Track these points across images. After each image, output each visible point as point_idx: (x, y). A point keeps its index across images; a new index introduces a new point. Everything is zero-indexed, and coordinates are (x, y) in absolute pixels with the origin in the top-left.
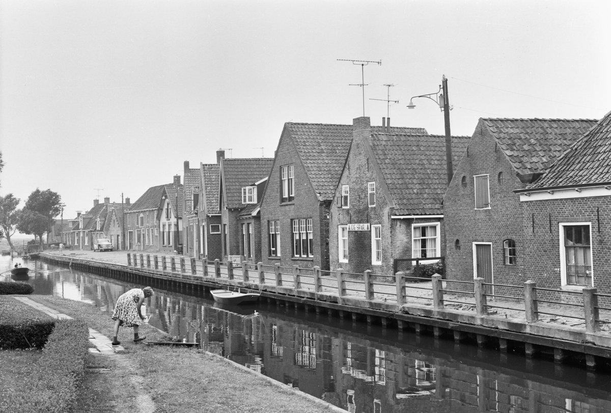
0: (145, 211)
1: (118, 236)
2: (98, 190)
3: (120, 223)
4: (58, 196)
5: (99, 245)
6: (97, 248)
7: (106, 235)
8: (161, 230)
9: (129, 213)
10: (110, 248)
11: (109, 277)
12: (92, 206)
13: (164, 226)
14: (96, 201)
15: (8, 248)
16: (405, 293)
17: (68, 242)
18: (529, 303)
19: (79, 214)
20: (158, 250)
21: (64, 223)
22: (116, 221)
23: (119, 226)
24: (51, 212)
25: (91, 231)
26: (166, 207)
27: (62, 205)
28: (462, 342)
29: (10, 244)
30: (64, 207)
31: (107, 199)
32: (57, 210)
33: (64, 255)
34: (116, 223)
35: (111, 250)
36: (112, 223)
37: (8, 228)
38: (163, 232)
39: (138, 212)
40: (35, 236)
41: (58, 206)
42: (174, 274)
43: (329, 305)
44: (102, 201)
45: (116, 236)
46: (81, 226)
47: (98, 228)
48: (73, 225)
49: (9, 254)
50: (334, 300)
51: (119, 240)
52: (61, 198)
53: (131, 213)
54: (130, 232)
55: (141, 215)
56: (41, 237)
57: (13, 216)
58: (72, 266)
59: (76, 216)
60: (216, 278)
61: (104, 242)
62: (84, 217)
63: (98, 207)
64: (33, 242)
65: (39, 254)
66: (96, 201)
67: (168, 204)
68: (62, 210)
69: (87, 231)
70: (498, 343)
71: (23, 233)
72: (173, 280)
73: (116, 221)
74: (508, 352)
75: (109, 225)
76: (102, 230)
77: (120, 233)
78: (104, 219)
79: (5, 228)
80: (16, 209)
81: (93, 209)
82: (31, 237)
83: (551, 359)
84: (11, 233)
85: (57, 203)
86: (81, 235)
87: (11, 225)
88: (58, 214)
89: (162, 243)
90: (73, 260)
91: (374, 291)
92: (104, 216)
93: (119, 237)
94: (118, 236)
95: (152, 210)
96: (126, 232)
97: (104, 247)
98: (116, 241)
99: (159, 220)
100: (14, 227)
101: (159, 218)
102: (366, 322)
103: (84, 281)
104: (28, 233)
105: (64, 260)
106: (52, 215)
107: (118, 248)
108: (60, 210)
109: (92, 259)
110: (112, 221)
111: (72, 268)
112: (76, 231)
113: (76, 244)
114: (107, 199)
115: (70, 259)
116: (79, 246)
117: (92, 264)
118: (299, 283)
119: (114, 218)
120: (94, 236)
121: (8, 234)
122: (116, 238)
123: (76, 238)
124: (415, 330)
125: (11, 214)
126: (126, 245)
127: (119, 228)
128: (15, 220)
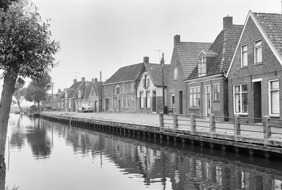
0: (121, 83)
1: (96, 102)
2: (76, 73)
3: (97, 93)
4: (50, 77)
5: (83, 108)
6: (81, 110)
7: (86, 101)
8: (138, 96)
9: (106, 86)
10: (91, 110)
11: (84, 128)
12: (72, 83)
13: (141, 93)
14: (75, 80)
15: (18, 110)
16: (163, 122)
17: (53, 107)
18: (53, 112)
19: (59, 91)
20: (134, 111)
21: (51, 96)
22: (94, 91)
23: (97, 95)
24: (45, 88)
25: (74, 99)
26: (144, 79)
27: (52, 83)
28: (226, 151)
29: (20, 107)
30: (53, 85)
31: (83, 79)
32: (49, 86)
33: (62, 114)
34: (94, 93)
35: (91, 112)
36: (91, 93)
37: (18, 98)
38: (140, 98)
39: (114, 84)
40: (35, 103)
41: (50, 84)
42: (176, 130)
43: (183, 136)
44: (79, 80)
45: (94, 102)
46: (66, 96)
47: (79, 97)
48: (56, 96)
49: (19, 113)
50: (188, 133)
51: (97, 104)
52: (52, 78)
53: (108, 85)
54: (106, 99)
55: (118, 86)
56: (39, 104)
57: (22, 91)
58: (71, 123)
59: (58, 92)
60: (236, 136)
61: (87, 106)
62: (68, 90)
63: (76, 84)
64: (34, 106)
65: (40, 113)
66: (75, 80)
67: (146, 76)
68: (53, 86)
69: (70, 99)
70: (249, 152)
71: (28, 101)
72: (74, 120)
73: (94, 91)
74: (253, 156)
75: (88, 95)
76: (82, 98)
77: (98, 100)
78: (83, 91)
79: (17, 98)
80: (23, 87)
81: (73, 85)
82: (32, 103)
83: (264, 157)
84: (20, 101)
85: (49, 82)
86: (66, 101)
87: (21, 97)
88: (50, 89)
89: (139, 106)
90: (73, 118)
91: (178, 124)
92: (83, 88)
93: (97, 103)
94: (96, 102)
95: (129, 82)
96: (103, 99)
97: (87, 109)
98: (95, 106)
99: (137, 89)
100: (22, 97)
101: (136, 87)
102: (200, 146)
103: (68, 132)
104: (31, 101)
105: (63, 118)
106: (46, 90)
107: (96, 110)
108: (51, 87)
109: (92, 118)
110: (91, 91)
111: (72, 125)
112: (63, 99)
113: (62, 108)
114: (83, 79)
115: (70, 118)
116: (65, 109)
117: (102, 123)
118: (177, 125)
119: (93, 89)
120: (76, 102)
121: (18, 102)
122: (94, 103)
123: (62, 104)
124: (191, 143)
125: (20, 90)
126: (103, 108)
127: (97, 96)
128: (23, 93)
